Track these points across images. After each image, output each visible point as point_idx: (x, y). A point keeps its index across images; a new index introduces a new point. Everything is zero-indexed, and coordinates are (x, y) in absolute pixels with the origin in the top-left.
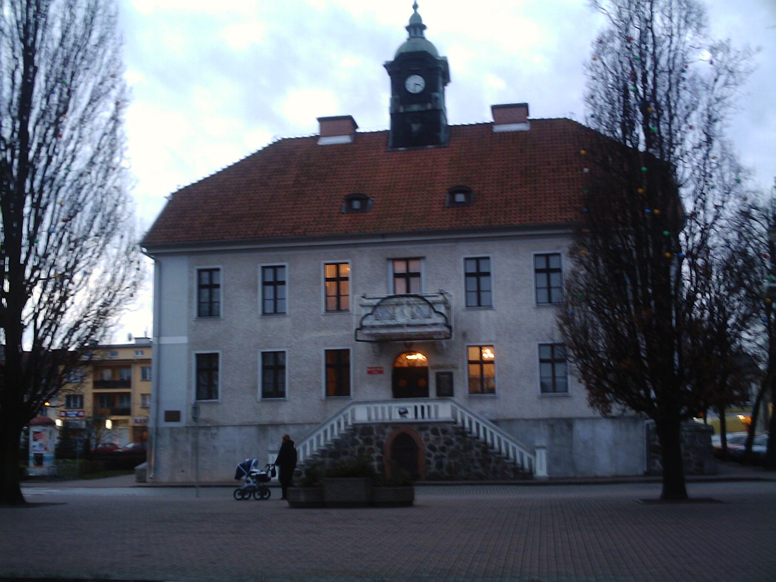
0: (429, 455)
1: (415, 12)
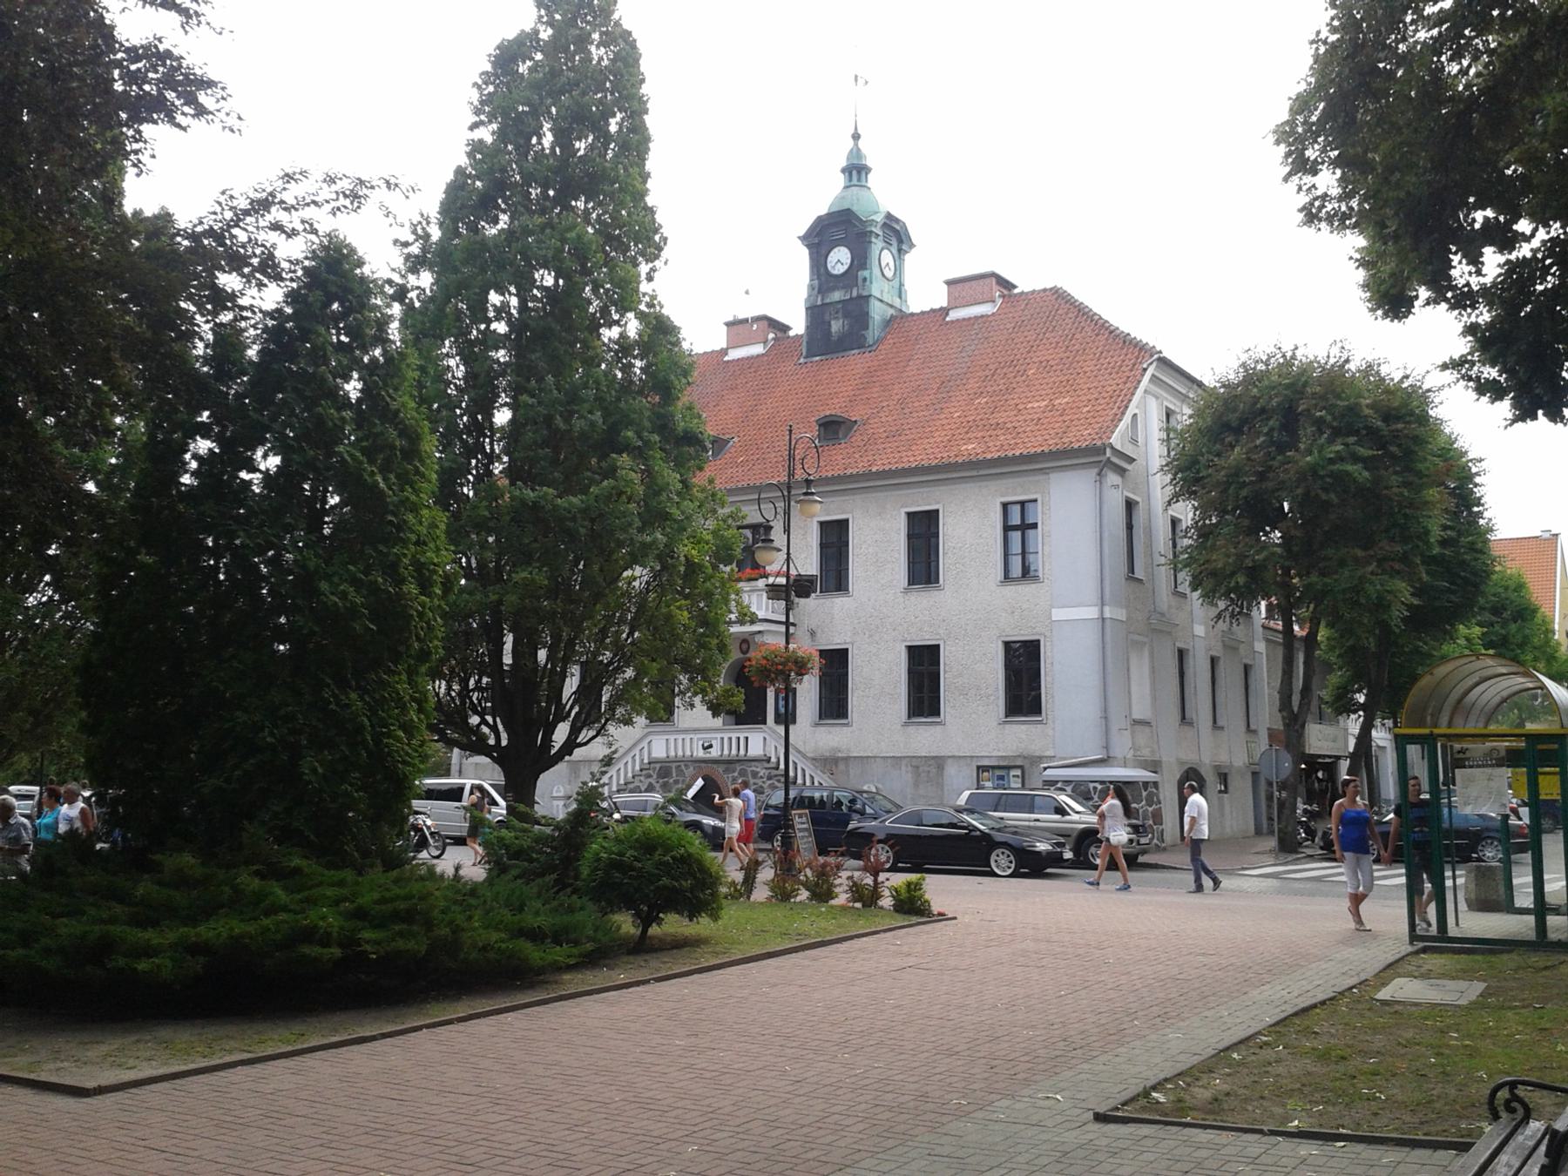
1: (856, 145)
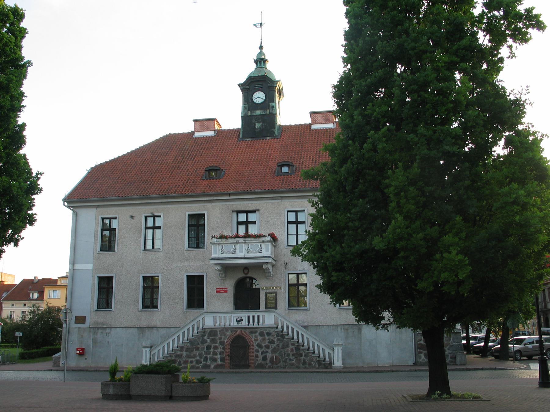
0: (258, 351)
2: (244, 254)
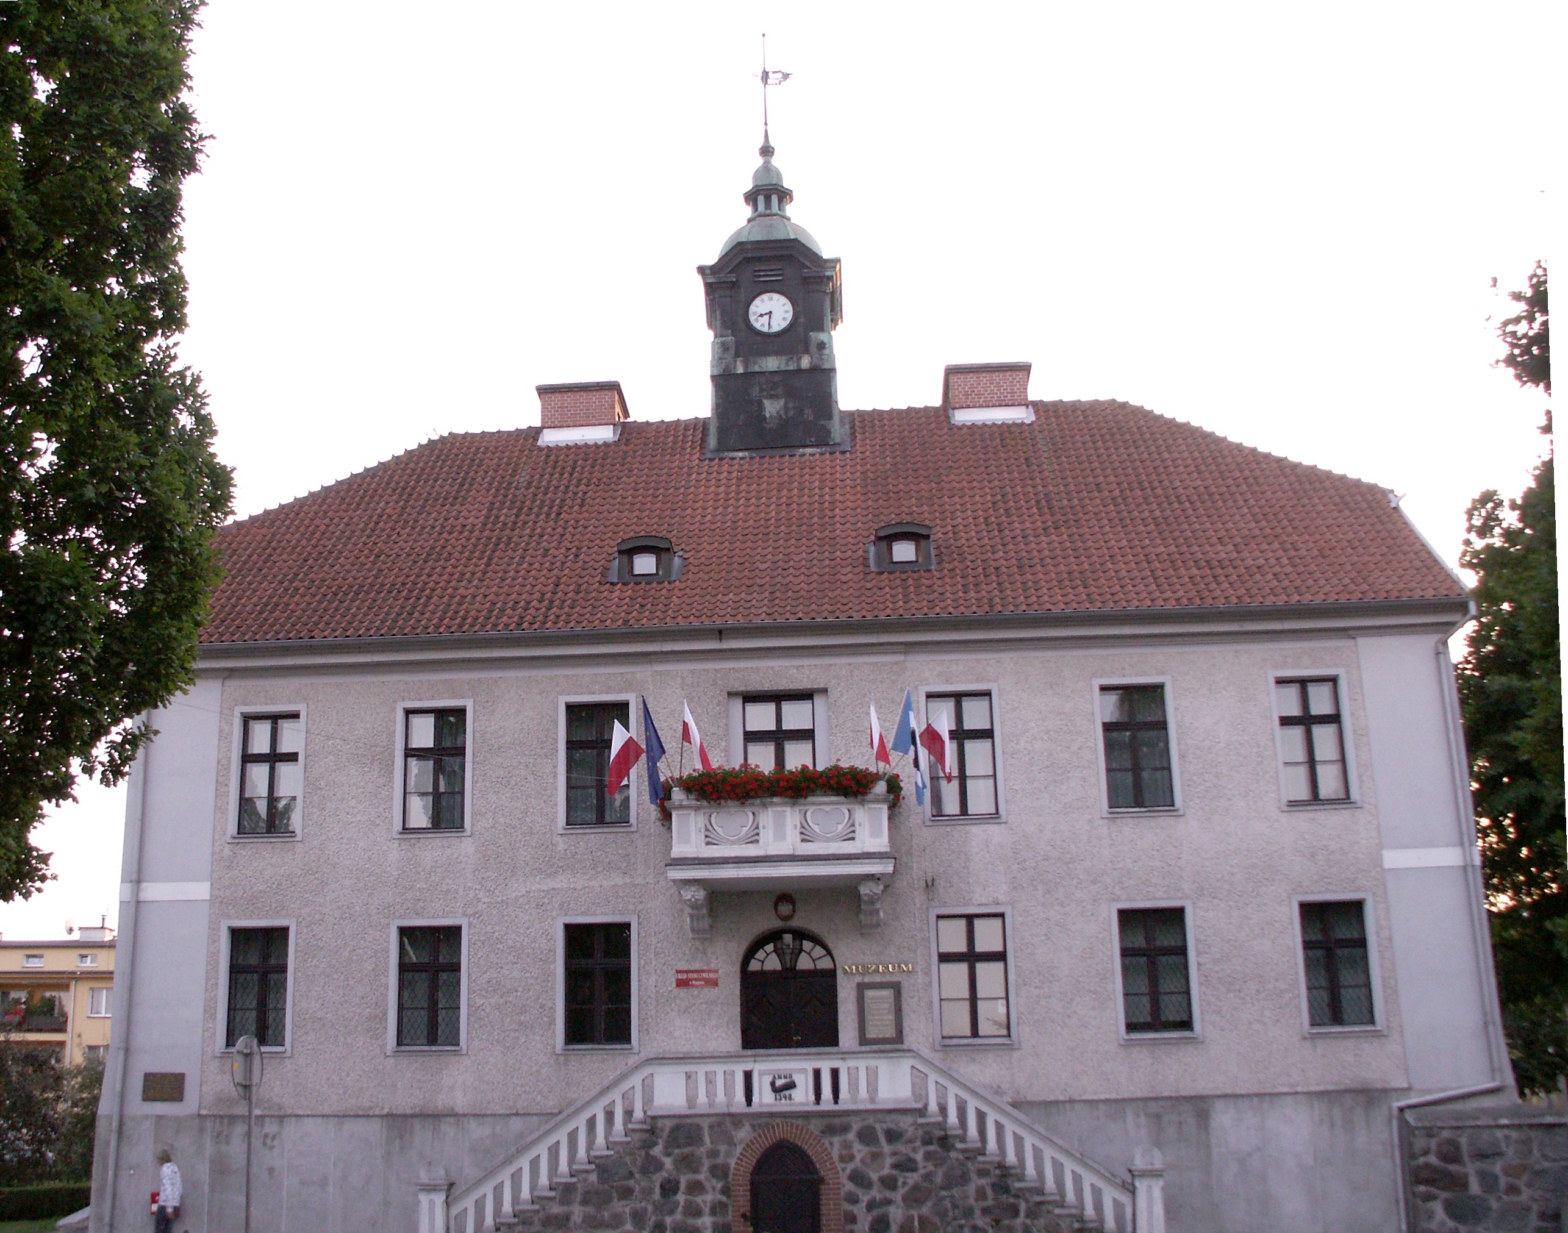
0: (854, 1200)
2: (790, 844)
